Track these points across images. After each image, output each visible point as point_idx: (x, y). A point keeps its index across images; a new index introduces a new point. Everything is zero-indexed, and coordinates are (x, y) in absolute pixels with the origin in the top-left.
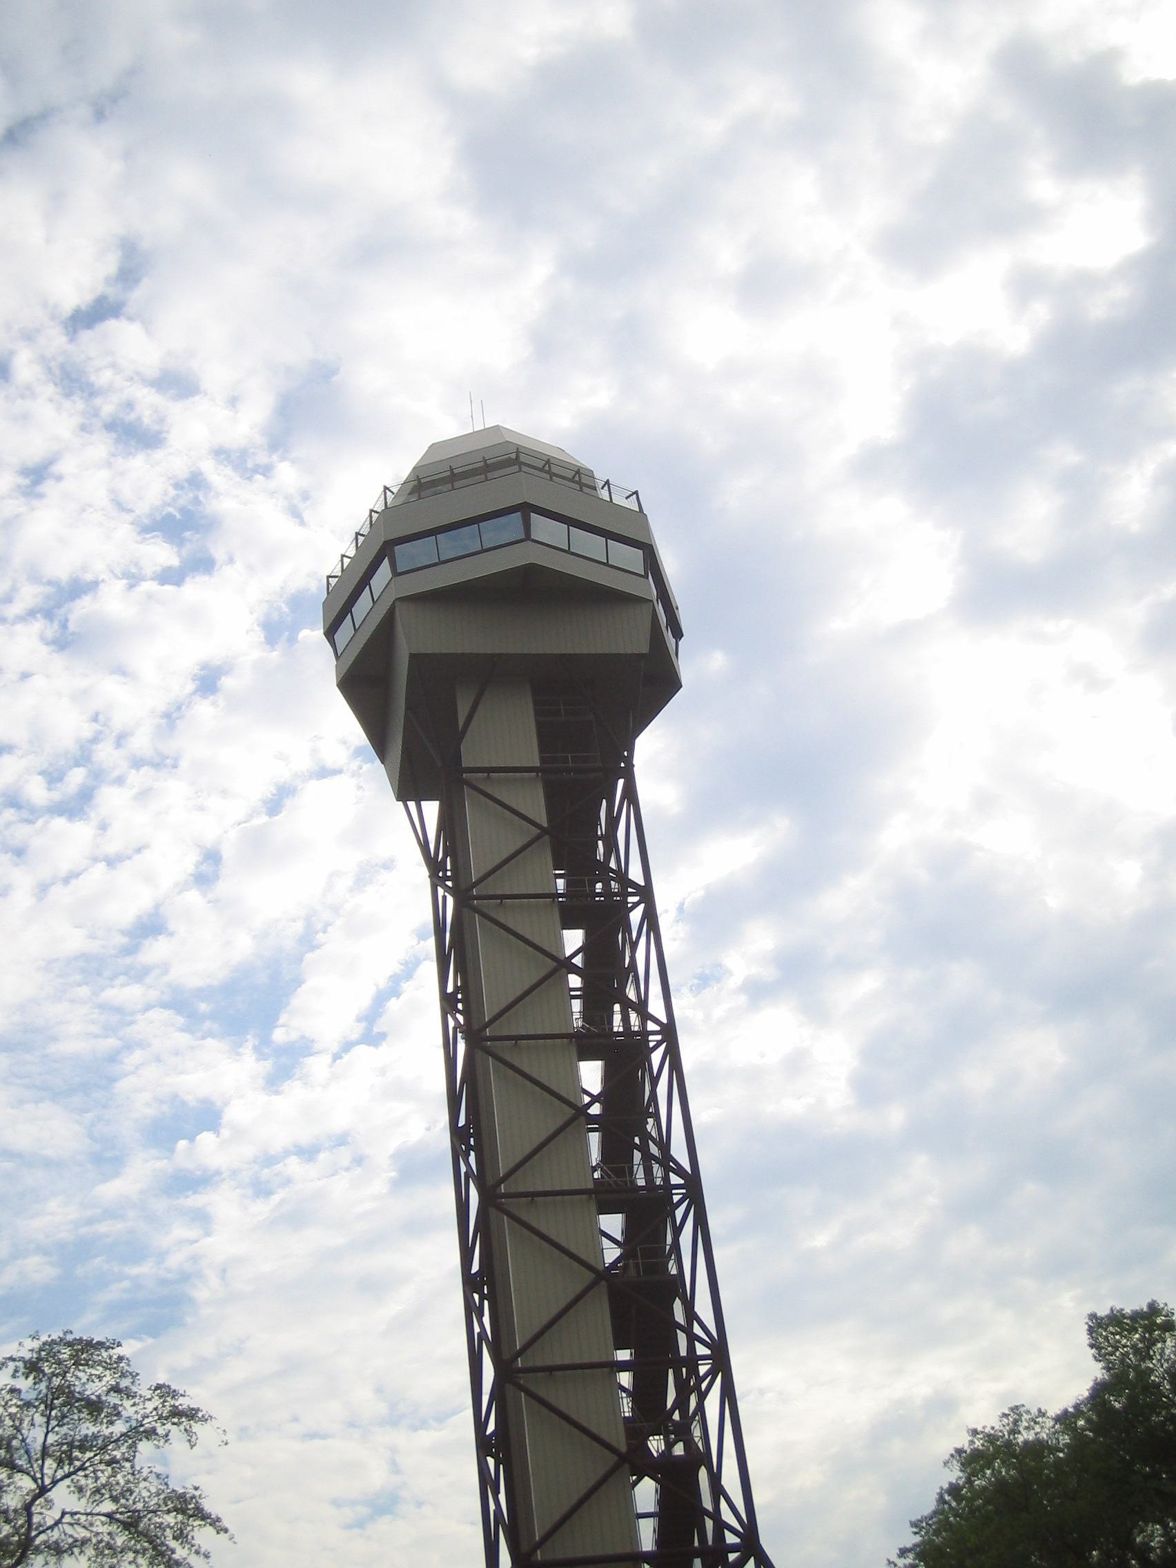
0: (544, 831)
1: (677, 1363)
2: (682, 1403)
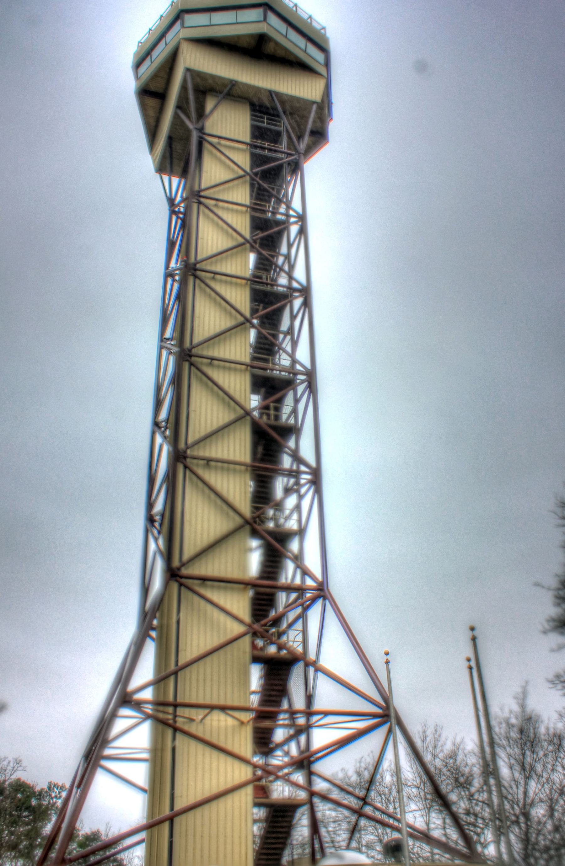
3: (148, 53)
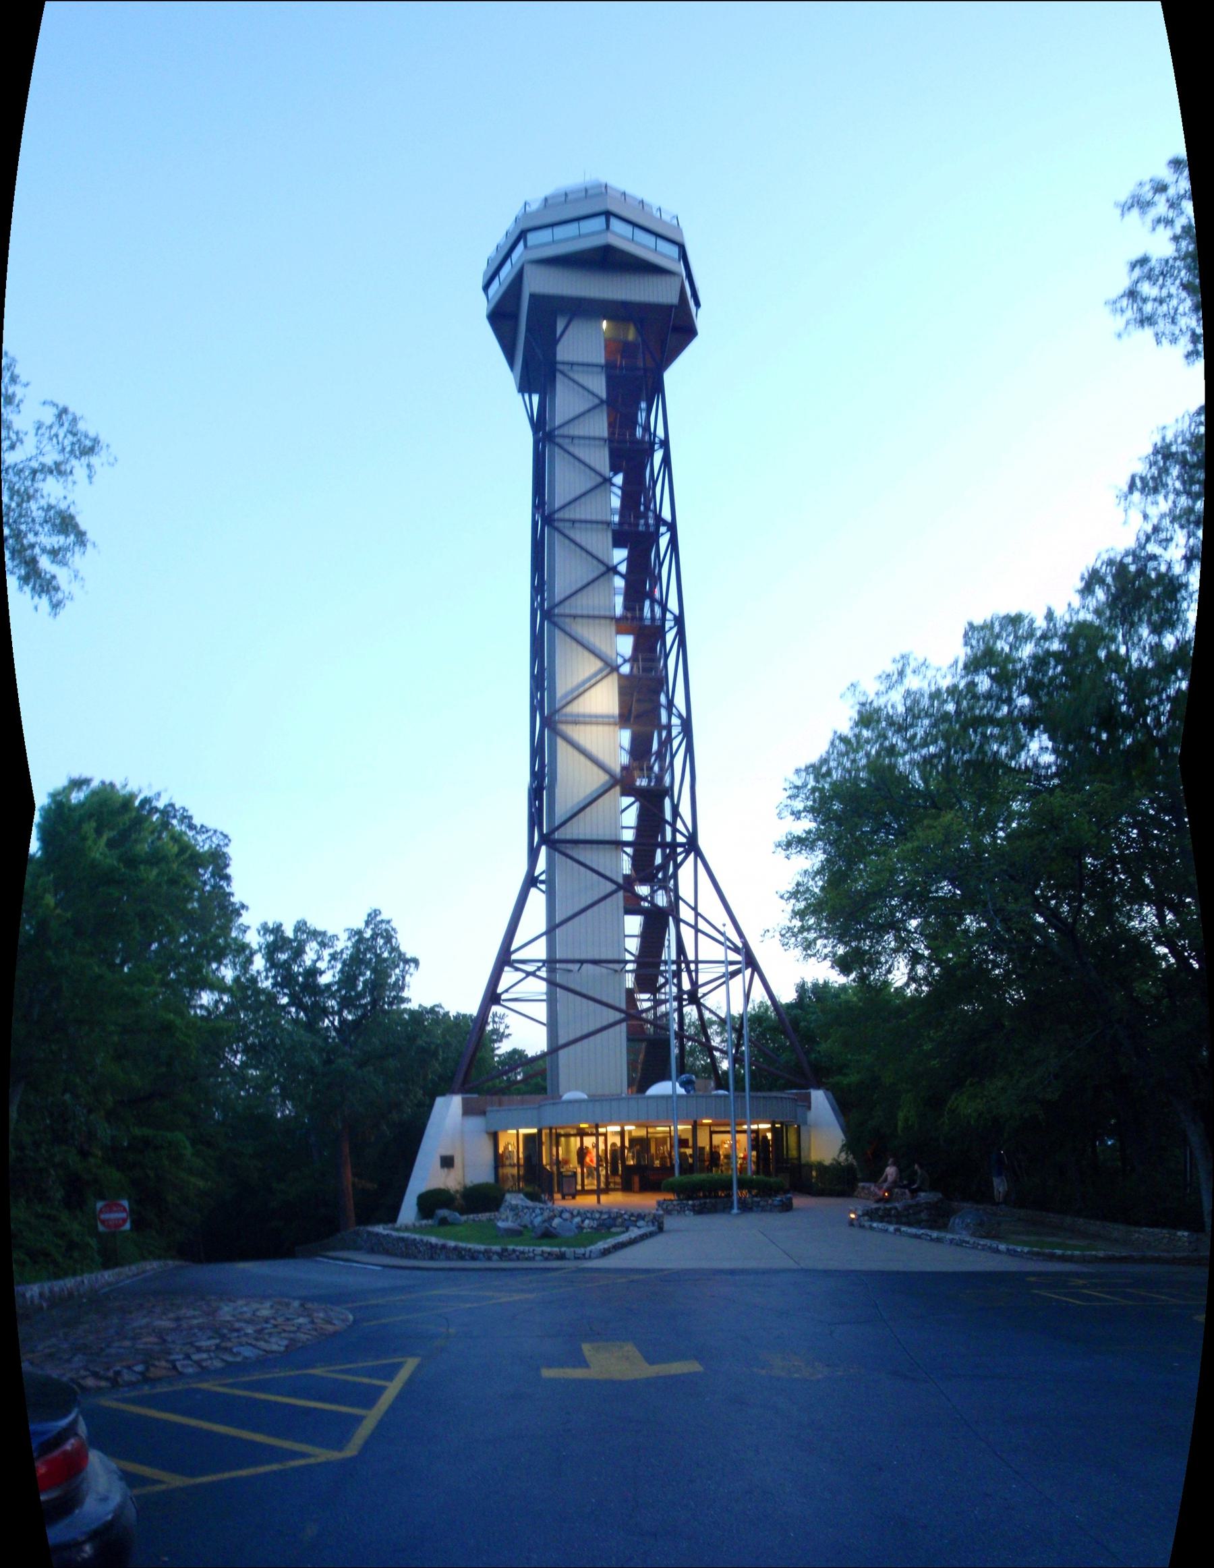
0: (602, 401)
1: (660, 728)
2: (664, 867)
3: (496, 272)
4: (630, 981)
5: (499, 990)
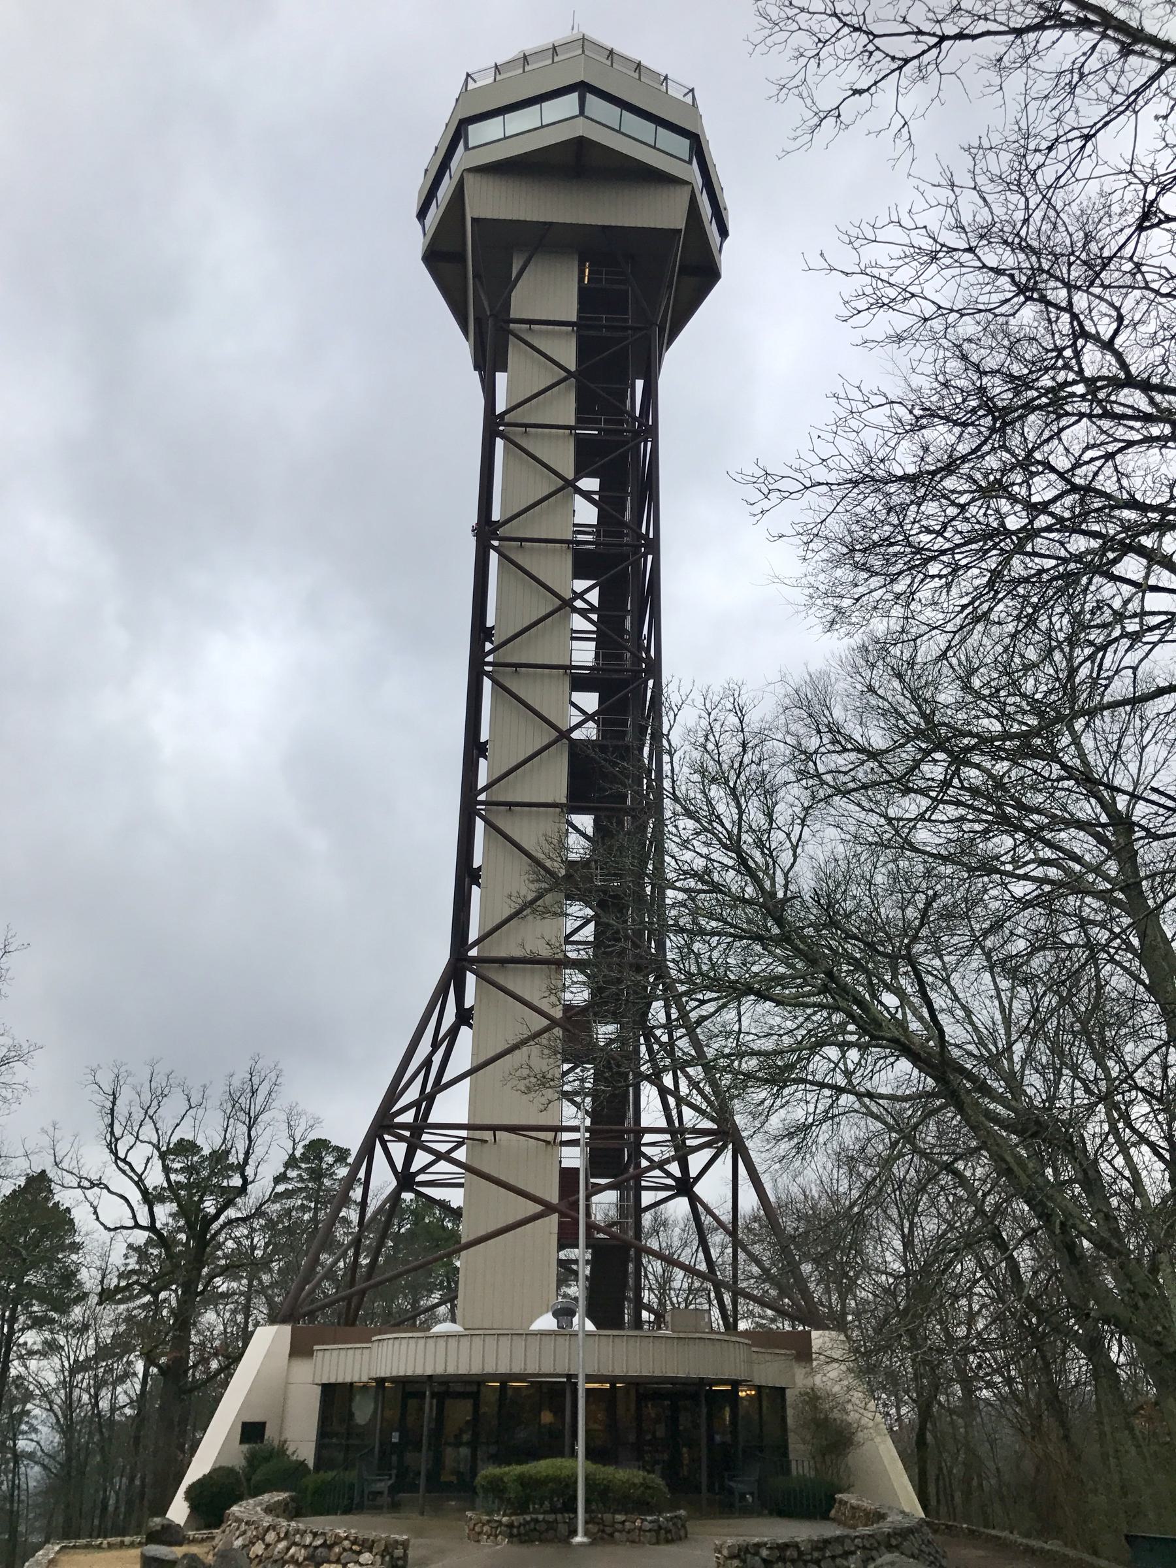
4: (573, 1158)
5: (413, 1169)
